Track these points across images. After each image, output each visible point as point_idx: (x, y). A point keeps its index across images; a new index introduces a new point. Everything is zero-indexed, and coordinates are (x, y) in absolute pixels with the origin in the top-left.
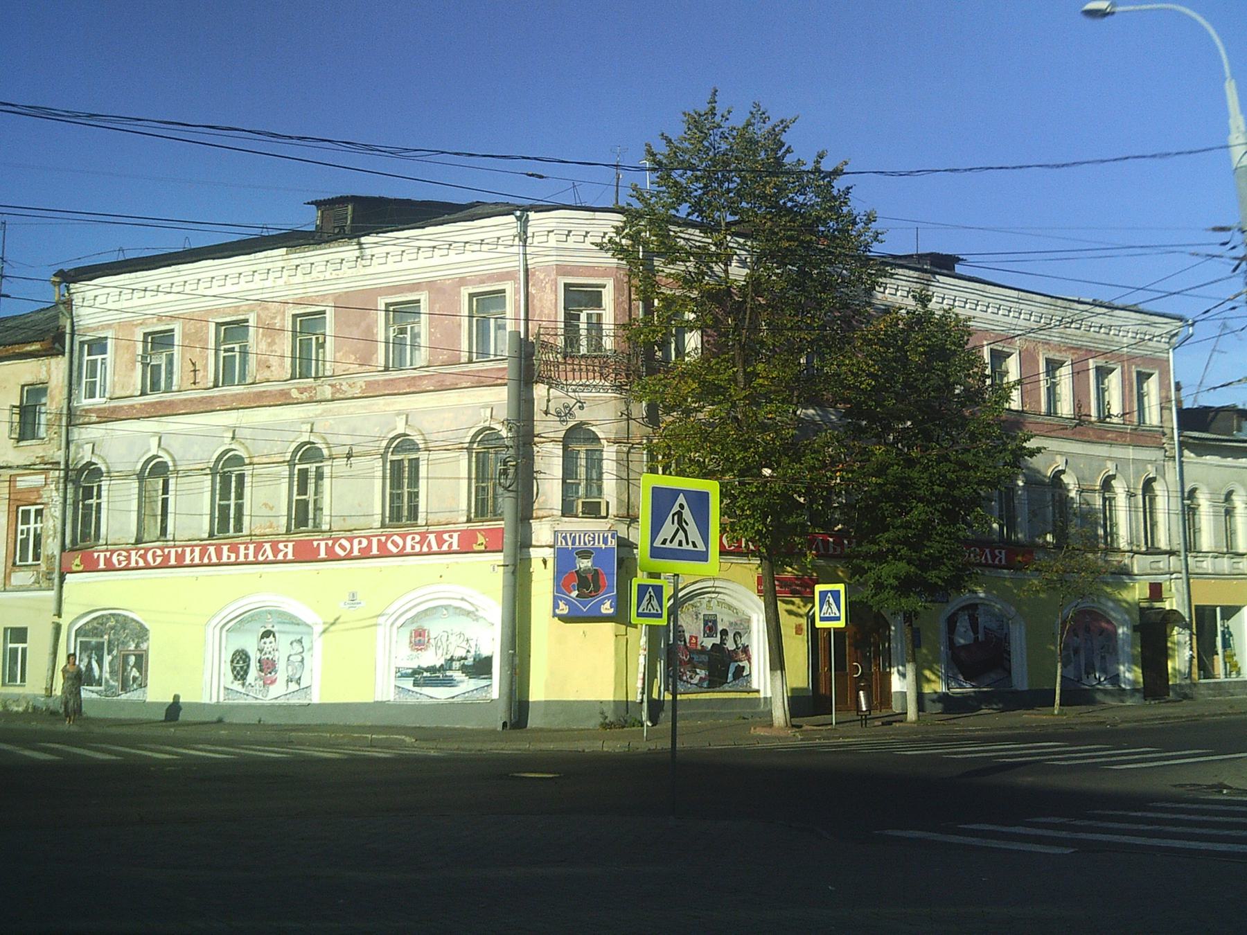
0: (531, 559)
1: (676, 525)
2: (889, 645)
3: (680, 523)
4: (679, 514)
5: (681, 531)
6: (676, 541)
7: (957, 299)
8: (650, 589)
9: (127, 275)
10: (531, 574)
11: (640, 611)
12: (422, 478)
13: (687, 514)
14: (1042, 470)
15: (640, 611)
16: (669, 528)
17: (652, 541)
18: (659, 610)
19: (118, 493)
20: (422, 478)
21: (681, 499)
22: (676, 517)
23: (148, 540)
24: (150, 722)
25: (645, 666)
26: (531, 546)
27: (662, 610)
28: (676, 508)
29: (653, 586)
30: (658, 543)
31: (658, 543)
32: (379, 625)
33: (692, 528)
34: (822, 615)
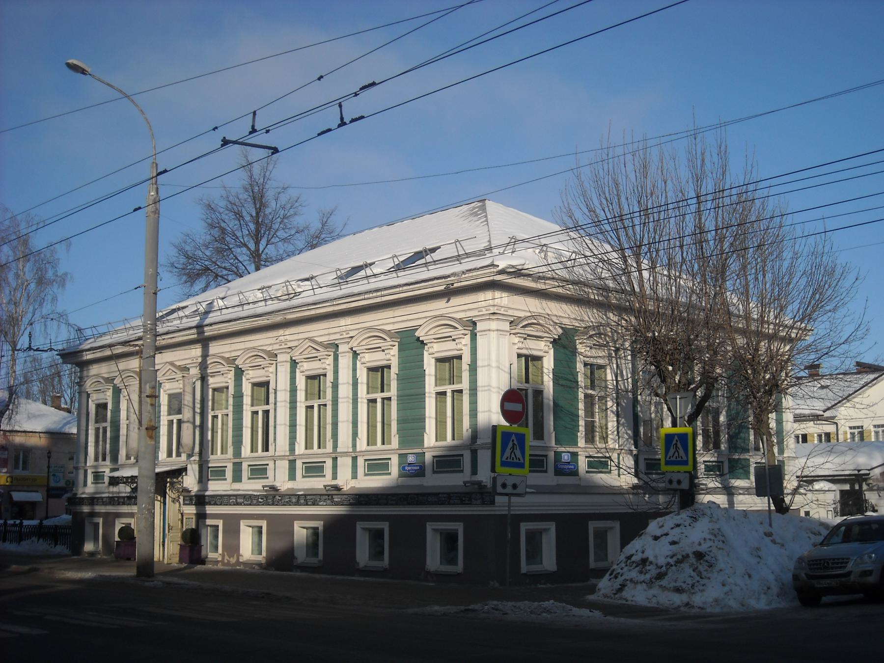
0: (289, 450)
1: (675, 449)
2: (740, 494)
3: (676, 449)
4: (676, 444)
6: (674, 457)
8: (513, 437)
9: (602, 512)
10: (201, 546)
13: (679, 445)
14: (773, 464)
15: (504, 459)
19: (494, 357)
25: (239, 490)
26: (208, 356)
27: (524, 460)
28: (674, 442)
29: (517, 435)
30: (667, 459)
34: (667, 459)
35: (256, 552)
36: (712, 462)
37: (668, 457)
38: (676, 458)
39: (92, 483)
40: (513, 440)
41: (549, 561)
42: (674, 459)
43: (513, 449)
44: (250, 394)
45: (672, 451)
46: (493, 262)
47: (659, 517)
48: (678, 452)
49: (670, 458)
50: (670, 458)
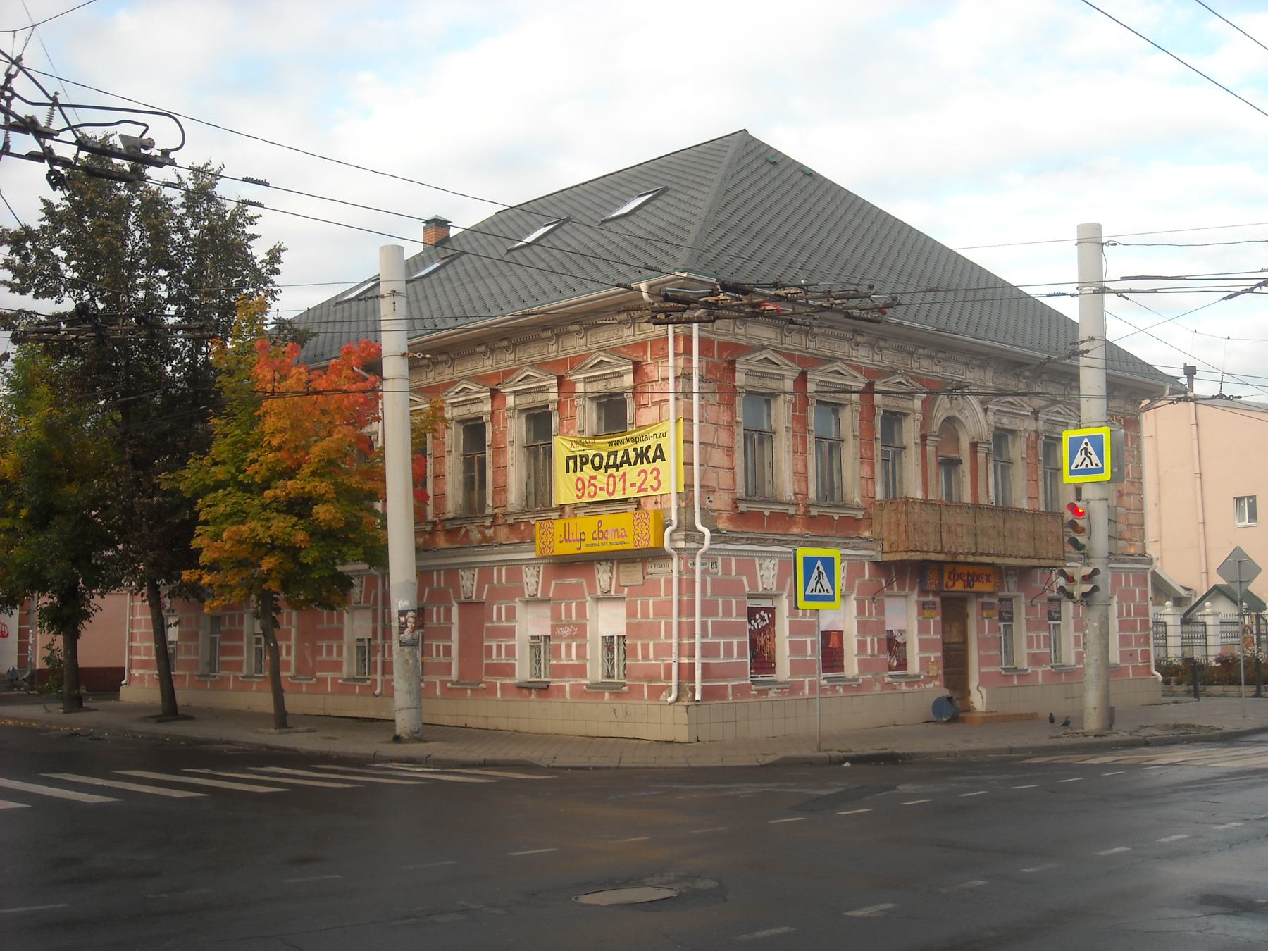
1: (1084, 456)
3: (1086, 454)
4: (1086, 449)
7: (1226, 378)
8: (819, 564)
11: (808, 592)
12: (1090, 397)
13: (1090, 449)
16: (1079, 458)
17: (1070, 466)
18: (830, 590)
20: (1090, 397)
22: (1083, 452)
23: (716, 481)
24: (902, 488)
28: (1083, 446)
29: (823, 560)
31: (1073, 468)
32: (1071, 344)
40: (818, 568)
43: (820, 579)
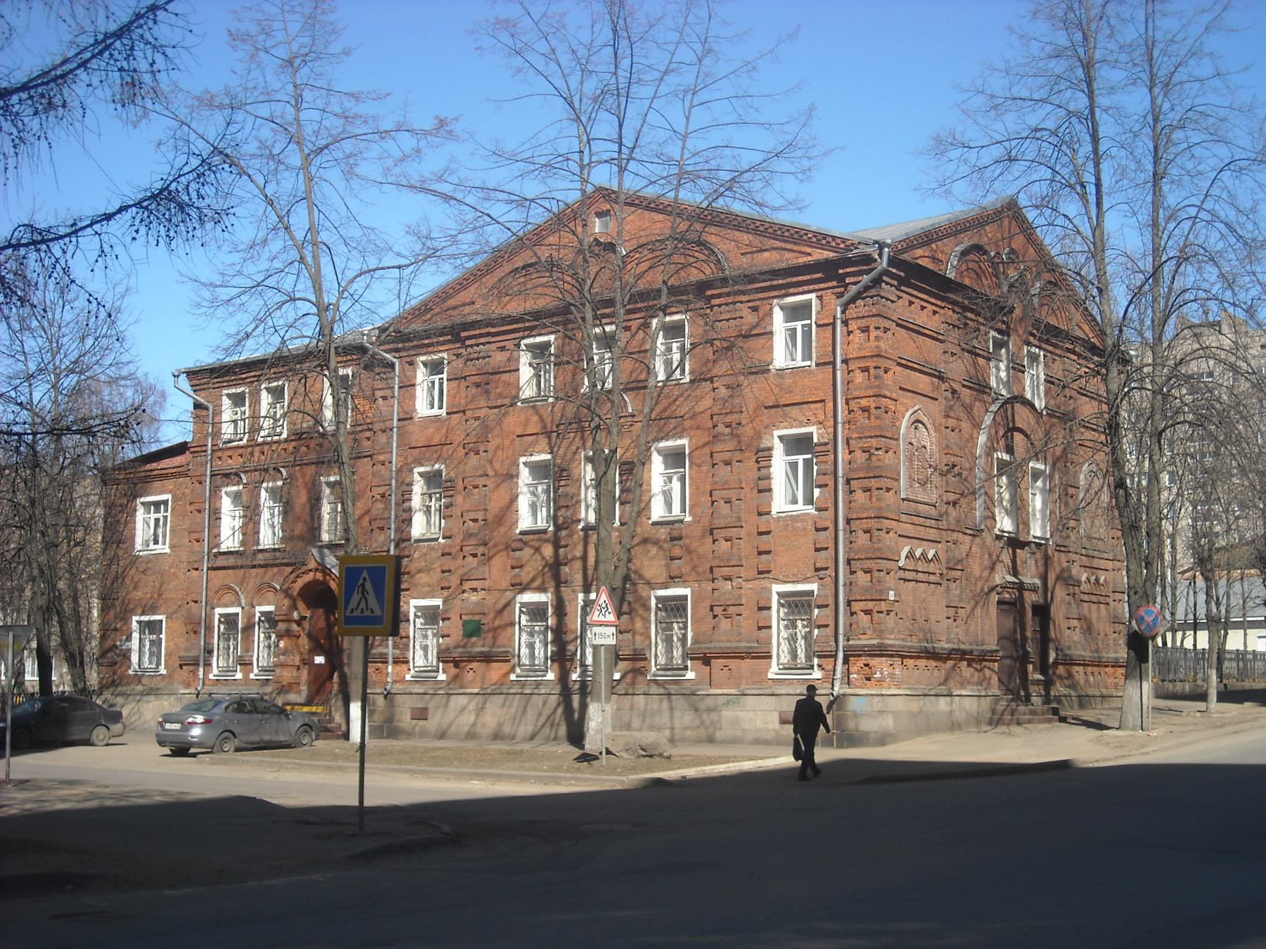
1: (360, 595)
3: (363, 593)
4: (363, 585)
5: (363, 601)
6: (359, 610)
13: (368, 586)
21: (365, 574)
28: (361, 581)
33: (371, 597)
34: (348, 613)
35: (789, 357)
36: (33, 664)
37: (349, 610)
38: (362, 612)
39: (770, 449)
41: (886, 250)
42: (357, 613)
44: (1104, 197)
45: (356, 597)
46: (265, 573)
47: (414, 401)
48: (366, 600)
49: (352, 612)
50: (352, 612)
